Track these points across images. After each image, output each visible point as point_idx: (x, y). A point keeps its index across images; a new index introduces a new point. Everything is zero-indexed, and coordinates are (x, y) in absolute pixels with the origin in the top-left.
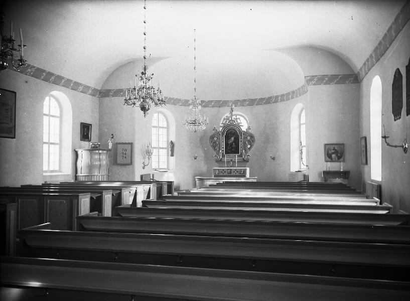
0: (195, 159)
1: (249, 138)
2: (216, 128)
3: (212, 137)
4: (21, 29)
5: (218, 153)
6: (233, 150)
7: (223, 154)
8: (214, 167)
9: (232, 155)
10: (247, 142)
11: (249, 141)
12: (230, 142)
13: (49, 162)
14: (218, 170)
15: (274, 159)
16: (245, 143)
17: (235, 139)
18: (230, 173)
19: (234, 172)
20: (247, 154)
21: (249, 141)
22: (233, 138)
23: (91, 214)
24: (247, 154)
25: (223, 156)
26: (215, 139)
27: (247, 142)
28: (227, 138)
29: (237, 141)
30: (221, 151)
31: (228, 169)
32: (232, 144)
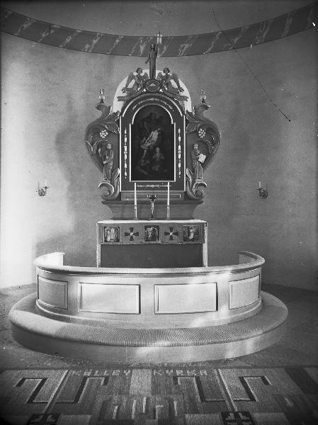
0: (42, 193)
1: (202, 133)
2: (106, 104)
3: (94, 129)
4: (144, 412)
5: (111, 177)
6: (156, 168)
7: (125, 180)
8: (99, 220)
9: (152, 183)
10: (196, 147)
11: (201, 142)
12: (147, 145)
13: (215, 343)
14: (117, 228)
15: (264, 195)
16: (190, 148)
17: (161, 135)
18: (154, 237)
19: (167, 234)
20: (198, 181)
21: (201, 142)
22: (155, 135)
23: (109, 296)
24: (198, 181)
25: (127, 186)
26: (103, 134)
27: (196, 147)
28: (139, 133)
29: (166, 142)
30: (120, 171)
31: (147, 227)
32: (151, 152)
